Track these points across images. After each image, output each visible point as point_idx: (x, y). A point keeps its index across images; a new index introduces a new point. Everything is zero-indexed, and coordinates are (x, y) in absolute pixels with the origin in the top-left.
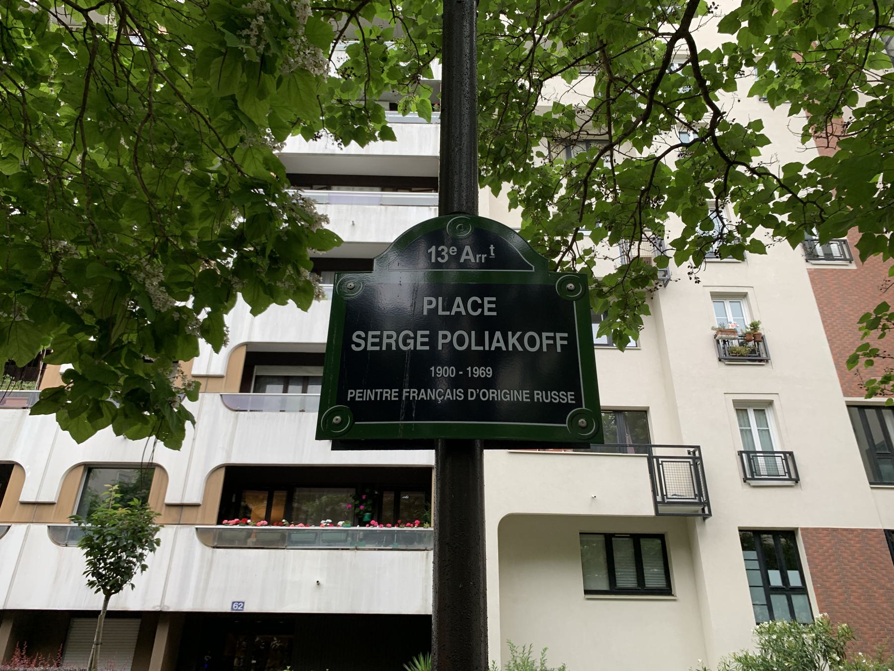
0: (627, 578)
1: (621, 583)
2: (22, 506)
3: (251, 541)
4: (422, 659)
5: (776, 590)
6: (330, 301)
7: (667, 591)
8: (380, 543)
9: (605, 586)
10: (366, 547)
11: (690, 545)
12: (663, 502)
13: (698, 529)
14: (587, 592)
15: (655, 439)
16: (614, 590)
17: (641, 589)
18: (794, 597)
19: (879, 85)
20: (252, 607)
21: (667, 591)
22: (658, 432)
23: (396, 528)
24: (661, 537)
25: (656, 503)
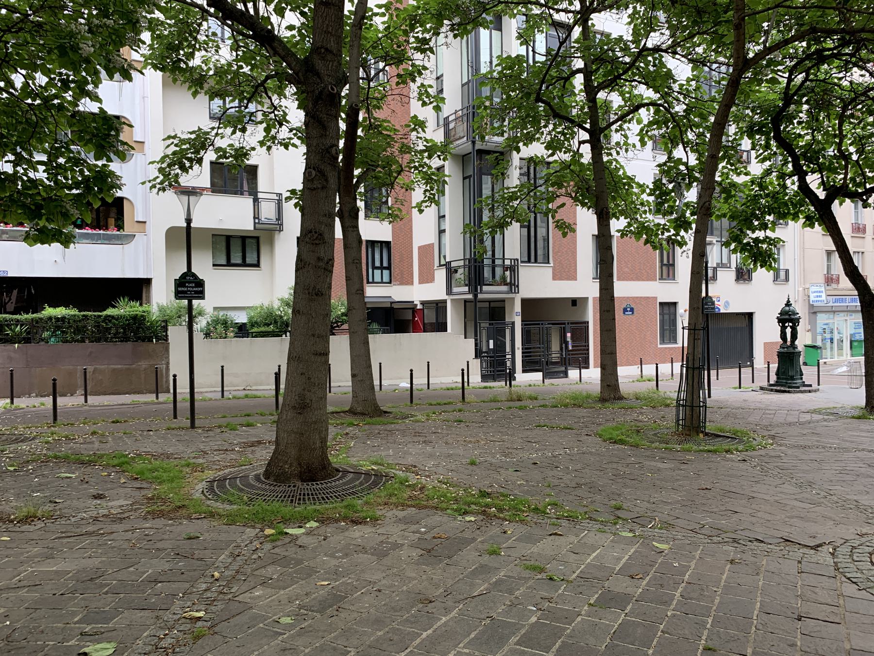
0: (236, 258)
1: (233, 261)
2: (136, 223)
3: (4, 236)
4: (126, 300)
5: (377, 268)
6: (481, 60)
7: (257, 265)
8: (93, 240)
9: (224, 263)
10: (117, 242)
11: (271, 243)
12: (259, 223)
13: (276, 236)
14: (214, 265)
15: (260, 189)
16: (229, 264)
17: (244, 264)
18: (384, 271)
19: (21, 69)
20: (11, 274)
21: (257, 265)
22: (263, 184)
23: (102, 232)
24: (257, 238)
25: (255, 223)
